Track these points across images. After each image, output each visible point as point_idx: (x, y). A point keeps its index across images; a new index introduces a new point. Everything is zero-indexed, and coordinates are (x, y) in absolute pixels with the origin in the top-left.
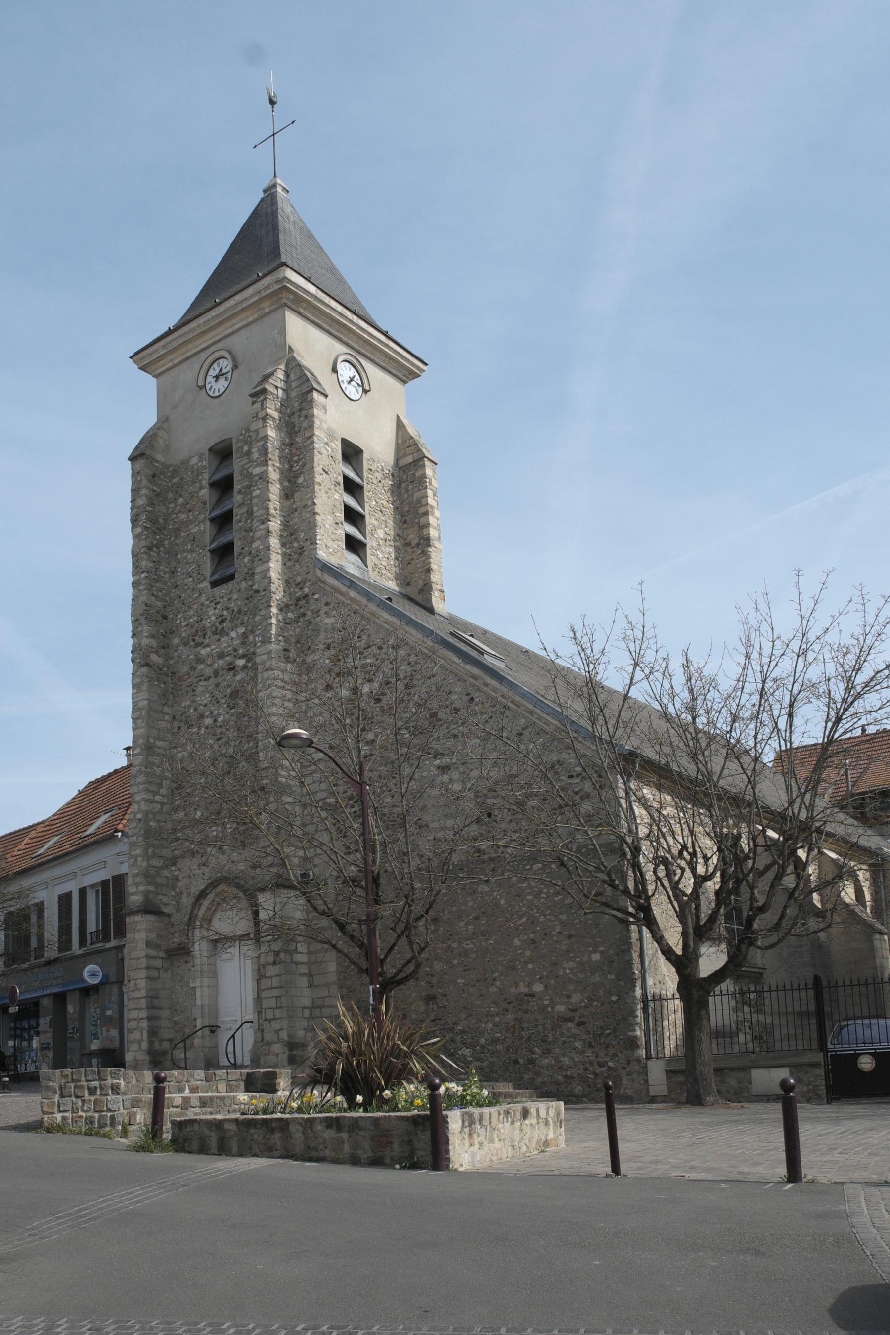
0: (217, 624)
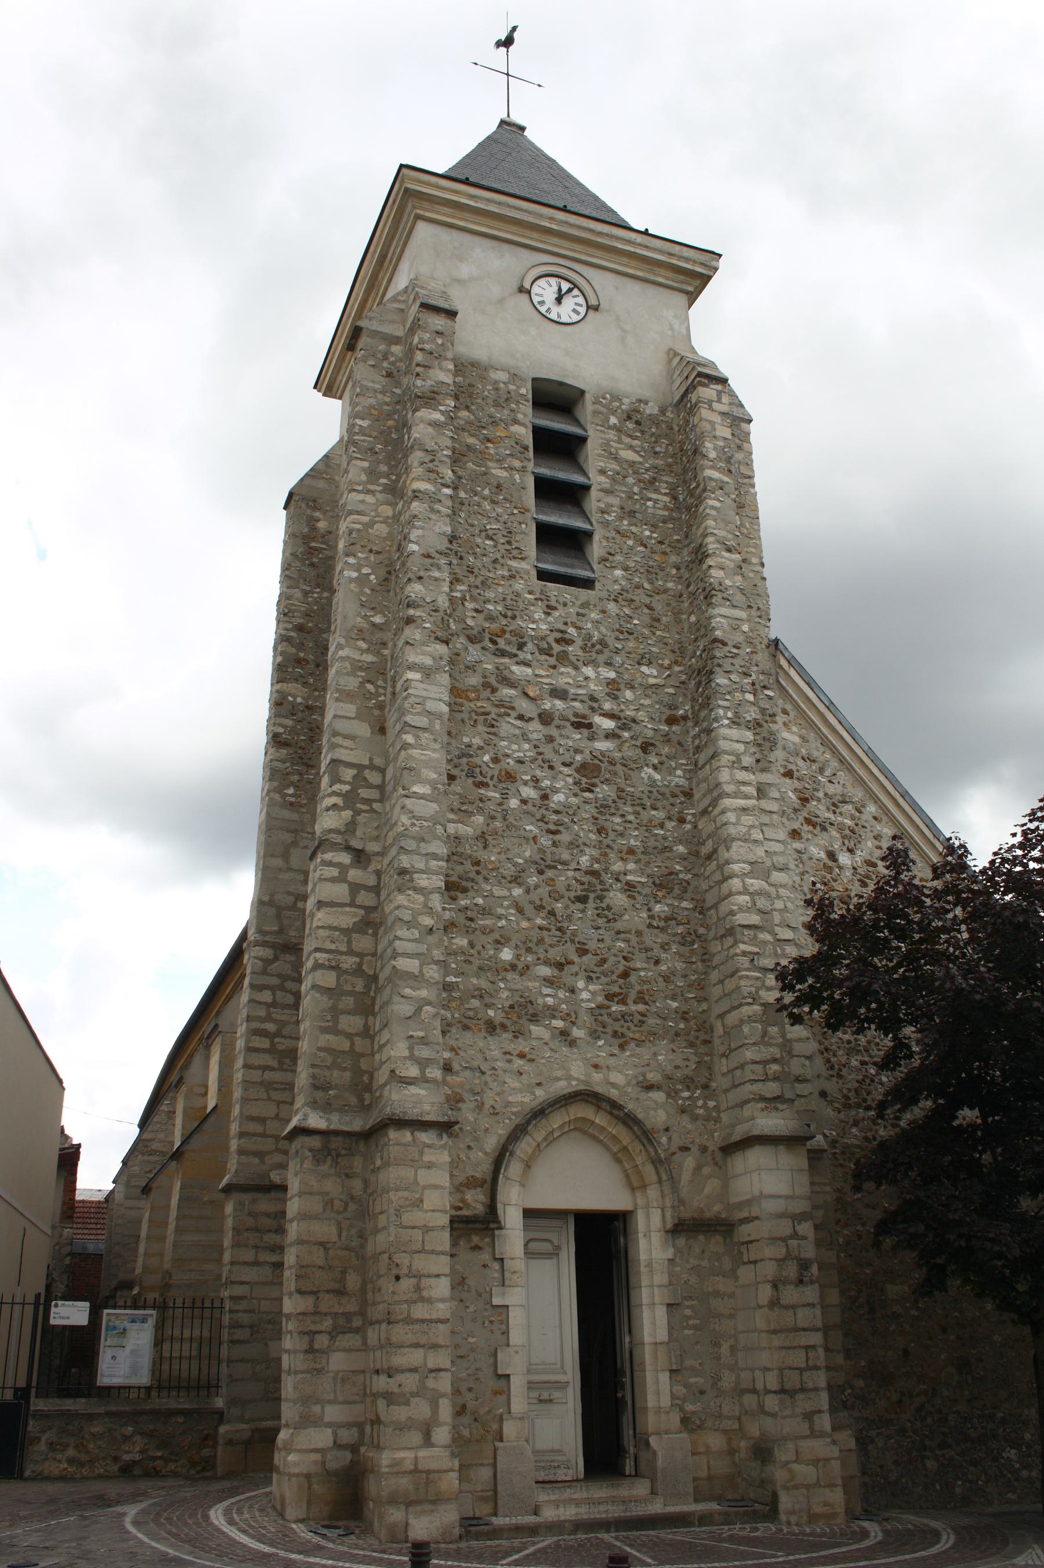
0: (551, 640)
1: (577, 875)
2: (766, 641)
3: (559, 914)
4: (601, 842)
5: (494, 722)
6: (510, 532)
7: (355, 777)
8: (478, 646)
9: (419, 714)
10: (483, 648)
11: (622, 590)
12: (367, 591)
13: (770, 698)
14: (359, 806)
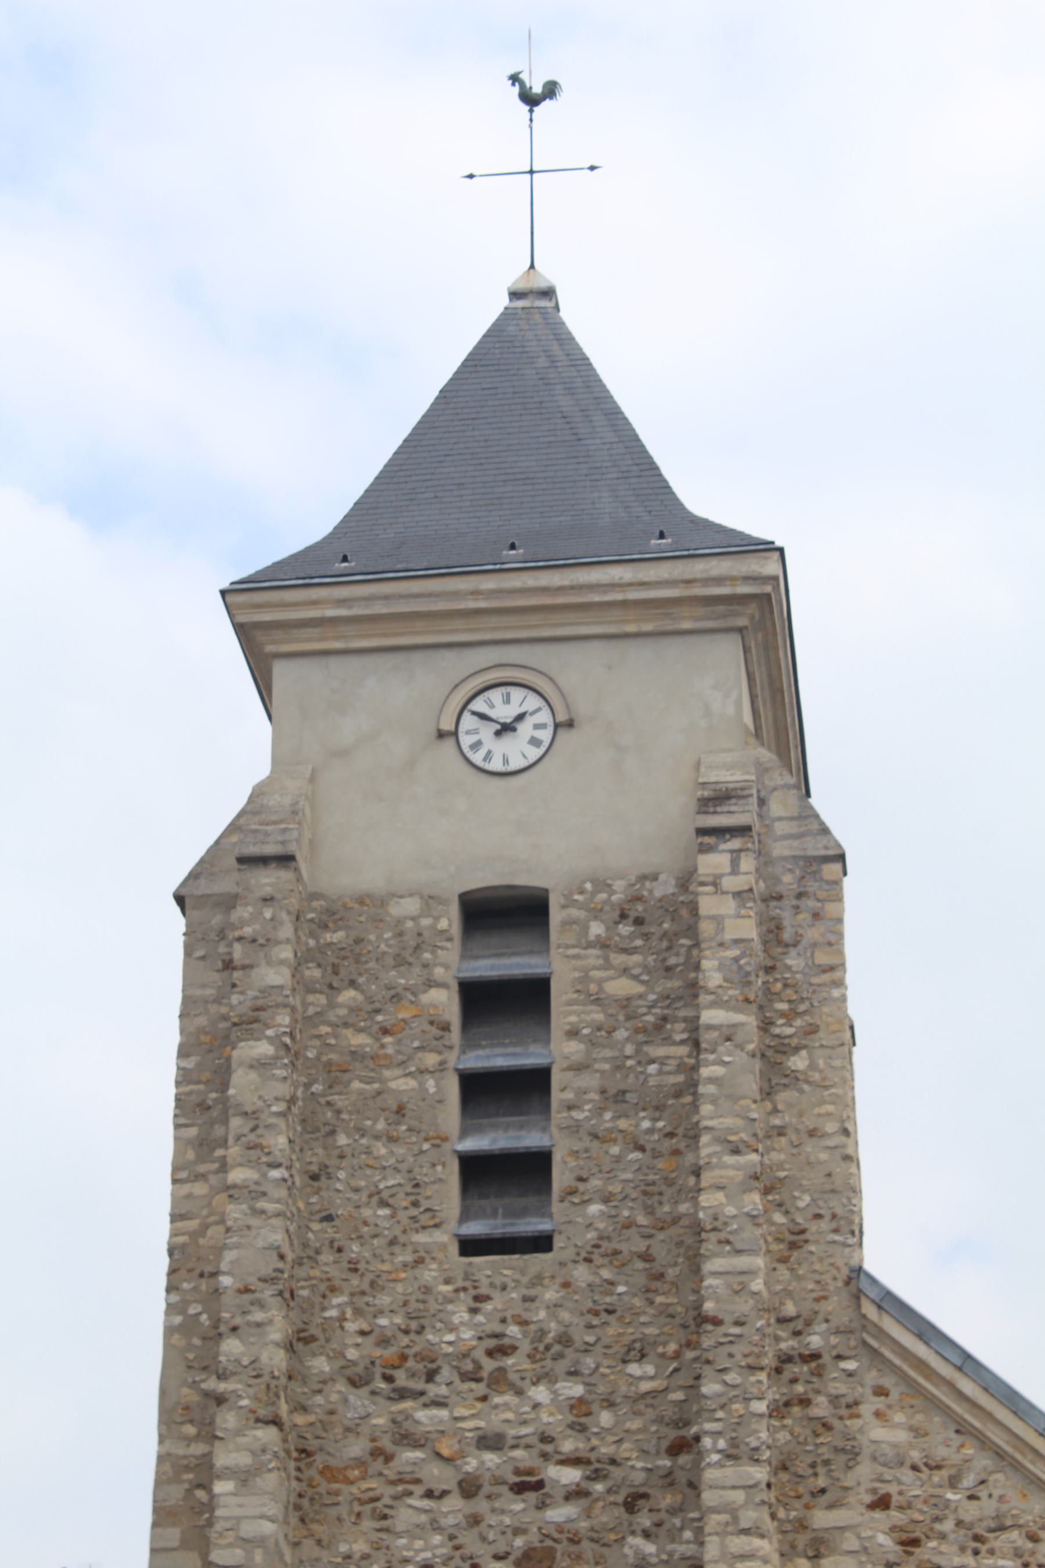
0: (479, 1354)
2: (845, 1272)
5: (387, 1511)
6: (417, 1185)
8: (364, 1391)
9: (230, 1545)
10: (373, 1393)
11: (601, 1238)
12: (197, 1341)
13: (850, 1374)
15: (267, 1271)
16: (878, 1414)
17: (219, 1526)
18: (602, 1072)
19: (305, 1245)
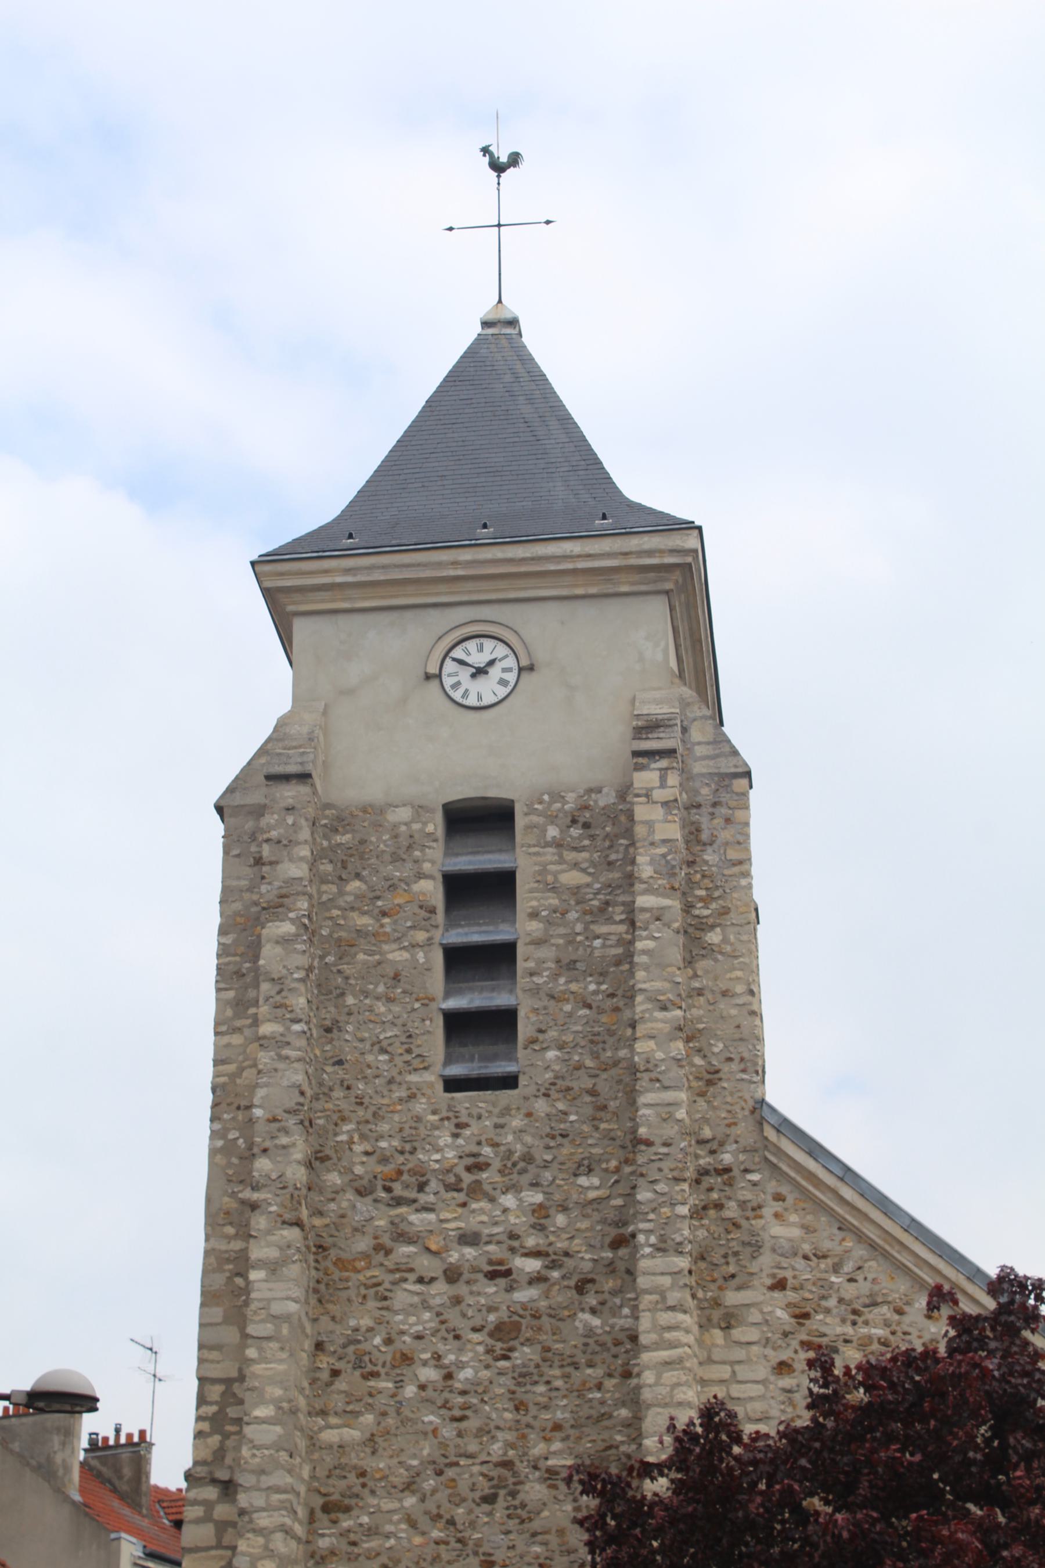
0: (460, 1170)
1: (484, 1469)
3: (459, 1520)
4: (518, 1421)
5: (387, 1294)
7: (223, 1394)
8: (369, 1199)
9: (262, 1321)
10: (376, 1201)
11: (556, 1077)
12: (235, 1160)
13: (755, 1184)
14: (229, 1428)
15: (291, 1104)
16: (776, 1215)
17: (253, 1306)
18: (557, 946)
19: (321, 1084)
